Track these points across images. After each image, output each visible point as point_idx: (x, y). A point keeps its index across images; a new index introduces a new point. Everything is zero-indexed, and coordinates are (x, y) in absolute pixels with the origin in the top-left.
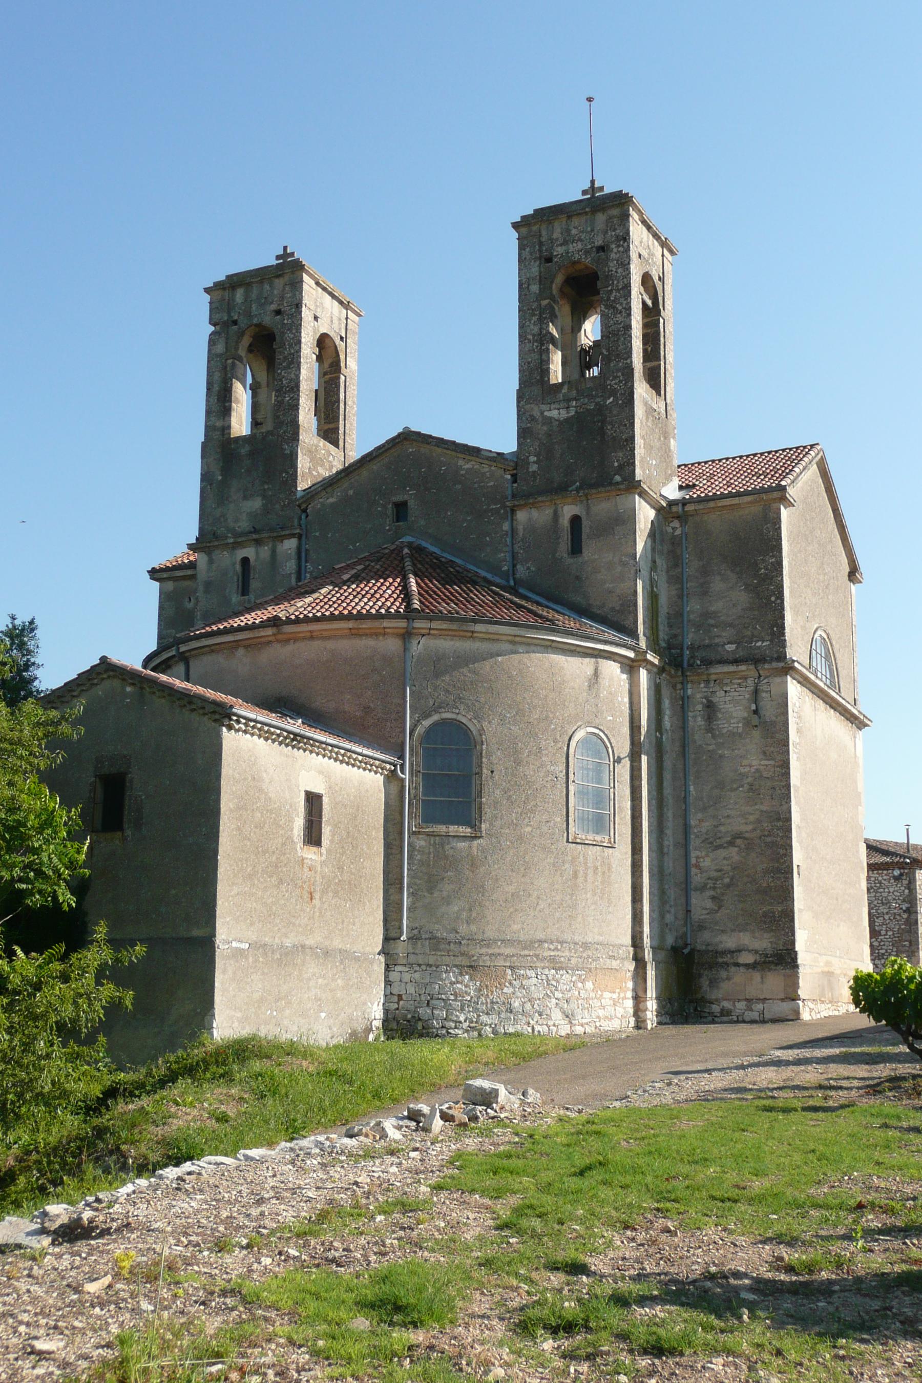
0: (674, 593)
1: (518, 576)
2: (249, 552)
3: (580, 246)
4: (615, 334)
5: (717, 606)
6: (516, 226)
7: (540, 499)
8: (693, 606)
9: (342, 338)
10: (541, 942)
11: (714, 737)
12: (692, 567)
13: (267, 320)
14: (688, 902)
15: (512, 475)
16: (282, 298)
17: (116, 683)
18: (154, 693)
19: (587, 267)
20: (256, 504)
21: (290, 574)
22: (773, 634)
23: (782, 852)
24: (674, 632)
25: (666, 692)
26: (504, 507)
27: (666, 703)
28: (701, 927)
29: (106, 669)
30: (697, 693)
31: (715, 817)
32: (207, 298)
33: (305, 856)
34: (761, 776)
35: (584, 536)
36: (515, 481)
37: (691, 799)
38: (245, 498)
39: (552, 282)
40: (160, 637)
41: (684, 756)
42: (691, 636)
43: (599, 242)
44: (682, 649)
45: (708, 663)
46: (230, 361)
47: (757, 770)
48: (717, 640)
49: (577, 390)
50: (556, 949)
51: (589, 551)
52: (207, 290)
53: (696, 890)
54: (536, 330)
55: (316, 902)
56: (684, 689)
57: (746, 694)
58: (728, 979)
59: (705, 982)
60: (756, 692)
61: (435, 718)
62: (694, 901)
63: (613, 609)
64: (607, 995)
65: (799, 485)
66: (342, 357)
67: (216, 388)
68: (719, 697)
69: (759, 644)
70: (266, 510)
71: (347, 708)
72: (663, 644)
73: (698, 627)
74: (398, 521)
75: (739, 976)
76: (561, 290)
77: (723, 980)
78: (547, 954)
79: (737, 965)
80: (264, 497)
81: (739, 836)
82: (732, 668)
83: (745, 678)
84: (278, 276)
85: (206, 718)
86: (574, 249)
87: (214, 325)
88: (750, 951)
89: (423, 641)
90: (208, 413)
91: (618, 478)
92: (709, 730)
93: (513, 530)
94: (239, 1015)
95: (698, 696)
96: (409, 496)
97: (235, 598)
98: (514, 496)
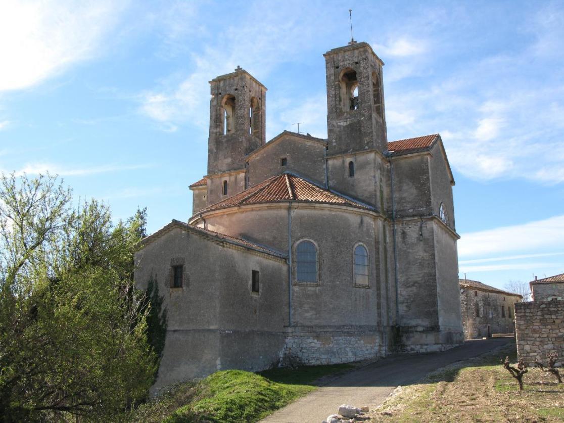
0: (388, 190)
1: (329, 185)
2: (227, 178)
3: (349, 62)
4: (364, 94)
5: (405, 195)
6: (324, 55)
7: (338, 156)
8: (396, 195)
9: (260, 99)
10: (344, 326)
11: (405, 245)
12: (395, 180)
13: (233, 92)
14: (397, 309)
15: (326, 147)
16: (238, 84)
17: (178, 230)
18: (193, 233)
19: (352, 70)
20: (229, 160)
21: (242, 187)
22: (427, 205)
23: (433, 288)
24: (389, 205)
25: (387, 228)
26: (323, 159)
27: (387, 232)
28: (403, 317)
29: (175, 223)
30: (398, 228)
31: (406, 275)
32: (210, 85)
33: (253, 296)
34: (424, 259)
35: (354, 169)
36: (327, 149)
37: (397, 269)
38: (225, 158)
39: (339, 75)
40: (194, 212)
41: (394, 252)
42: (395, 206)
43: (356, 60)
44: (392, 212)
45: (403, 217)
46: (218, 108)
47: (423, 257)
48: (406, 208)
49: (350, 115)
50: (349, 328)
51: (357, 175)
52: (209, 82)
53: (400, 303)
54: (334, 93)
55: (258, 313)
56: (394, 227)
57: (417, 228)
58: (413, 337)
59: (404, 339)
60: (421, 227)
61: (301, 240)
62: (399, 308)
63: (366, 197)
64: (369, 345)
65: (434, 149)
66: (260, 105)
67: (213, 118)
68: (408, 230)
69: (422, 209)
70: (233, 163)
71: (267, 237)
72: (385, 210)
73: (398, 203)
74: (283, 165)
75: (417, 336)
76: (342, 79)
77: (411, 337)
78: (346, 330)
79: (416, 331)
80: (232, 157)
81: (416, 282)
82: (412, 218)
83: (417, 222)
84: (236, 76)
85: (213, 243)
86: (347, 62)
87: (213, 95)
88: (421, 326)
89: (296, 211)
90: (211, 127)
91: (367, 147)
92: (404, 242)
93: (327, 168)
94: (229, 359)
95: (399, 229)
96: (287, 156)
97: (222, 196)
98: (327, 155)
